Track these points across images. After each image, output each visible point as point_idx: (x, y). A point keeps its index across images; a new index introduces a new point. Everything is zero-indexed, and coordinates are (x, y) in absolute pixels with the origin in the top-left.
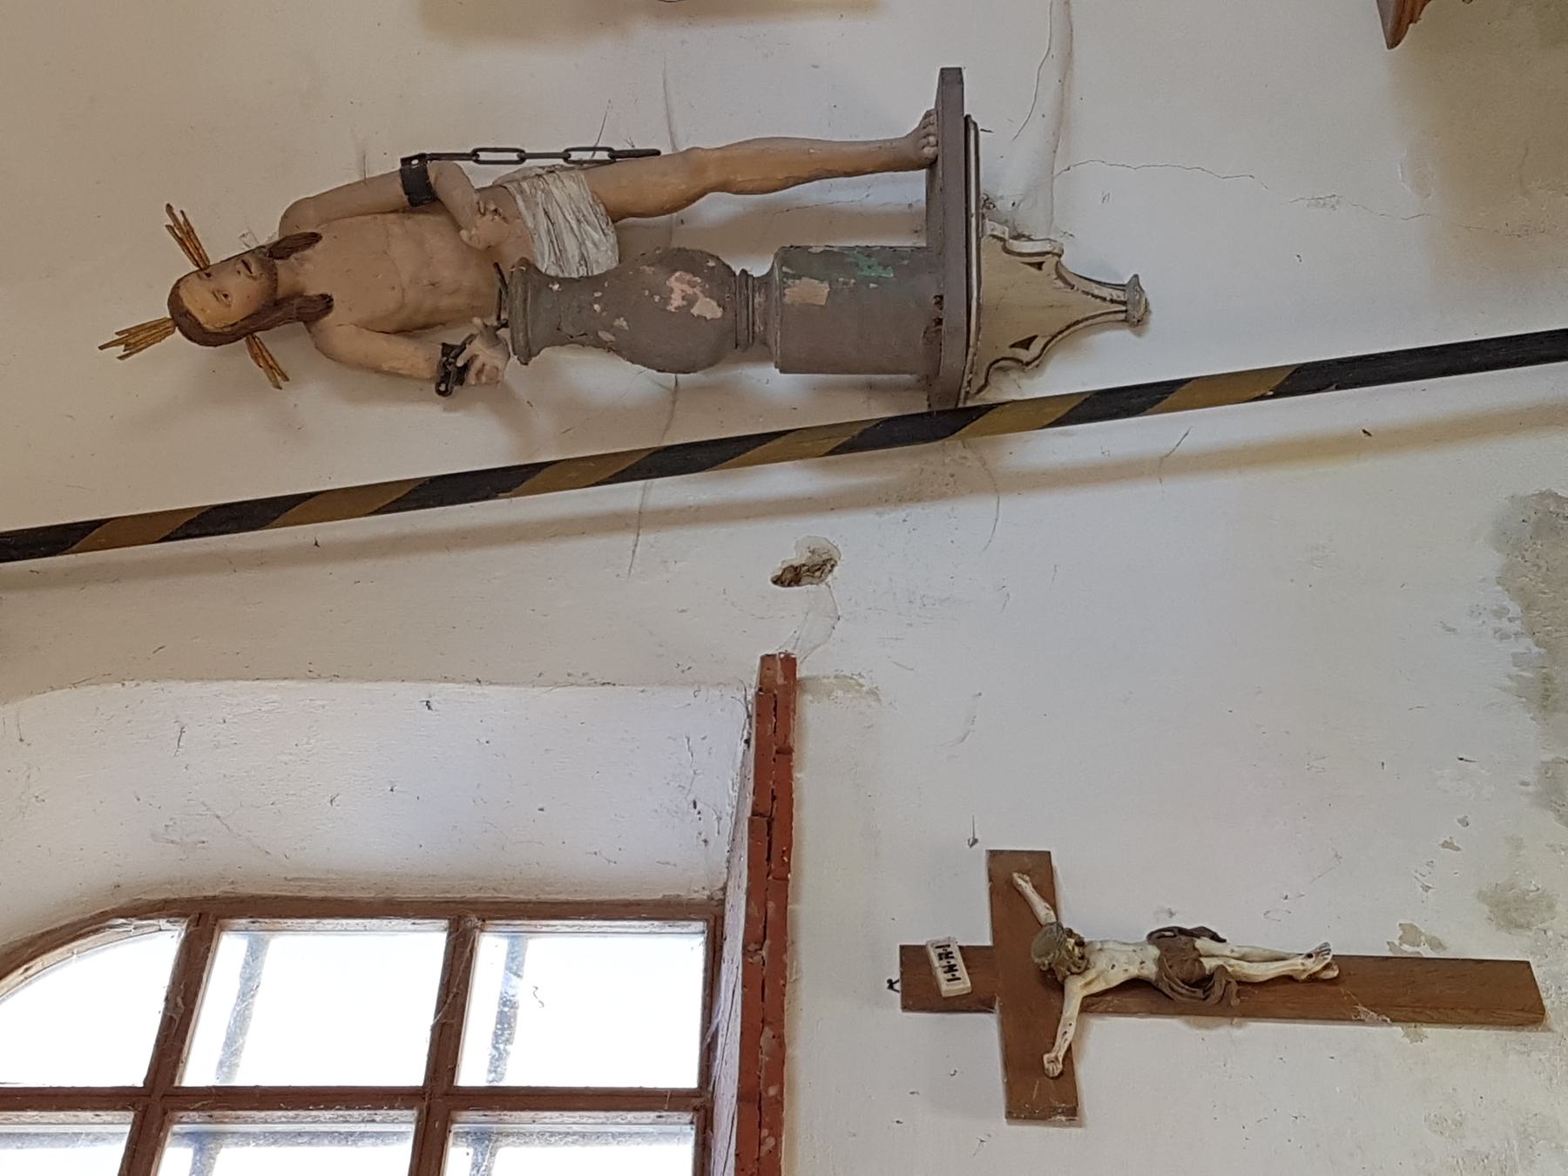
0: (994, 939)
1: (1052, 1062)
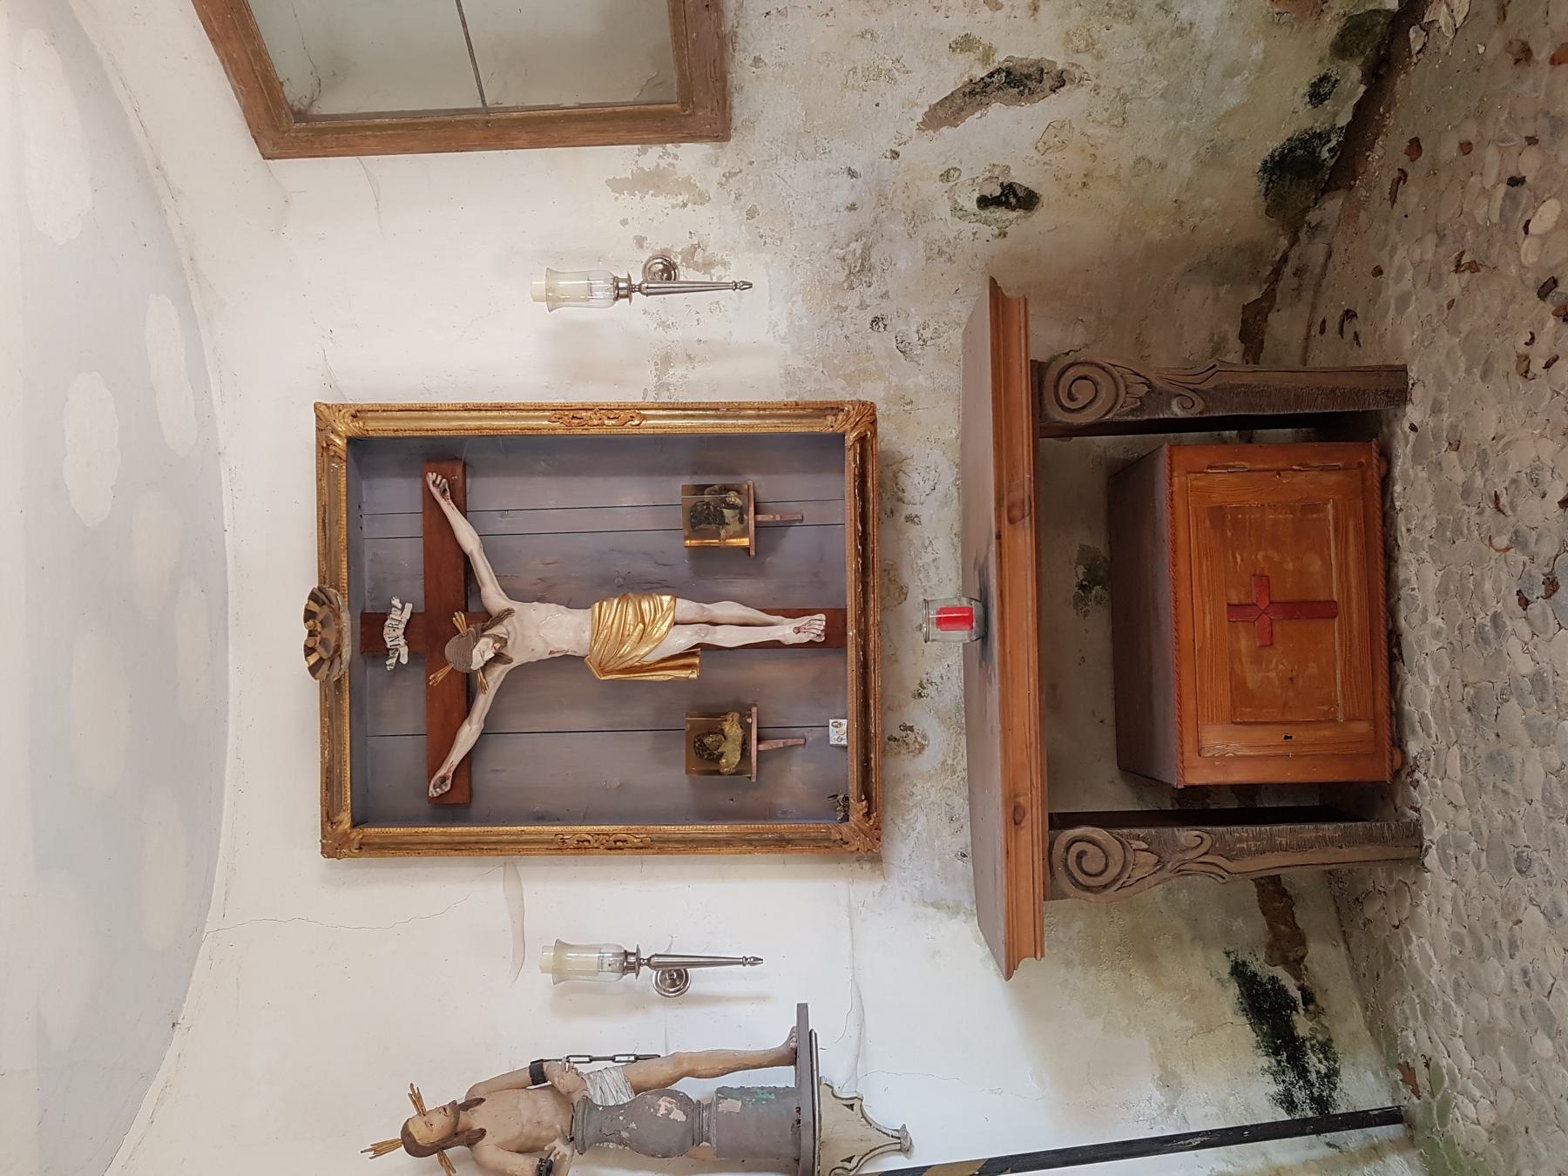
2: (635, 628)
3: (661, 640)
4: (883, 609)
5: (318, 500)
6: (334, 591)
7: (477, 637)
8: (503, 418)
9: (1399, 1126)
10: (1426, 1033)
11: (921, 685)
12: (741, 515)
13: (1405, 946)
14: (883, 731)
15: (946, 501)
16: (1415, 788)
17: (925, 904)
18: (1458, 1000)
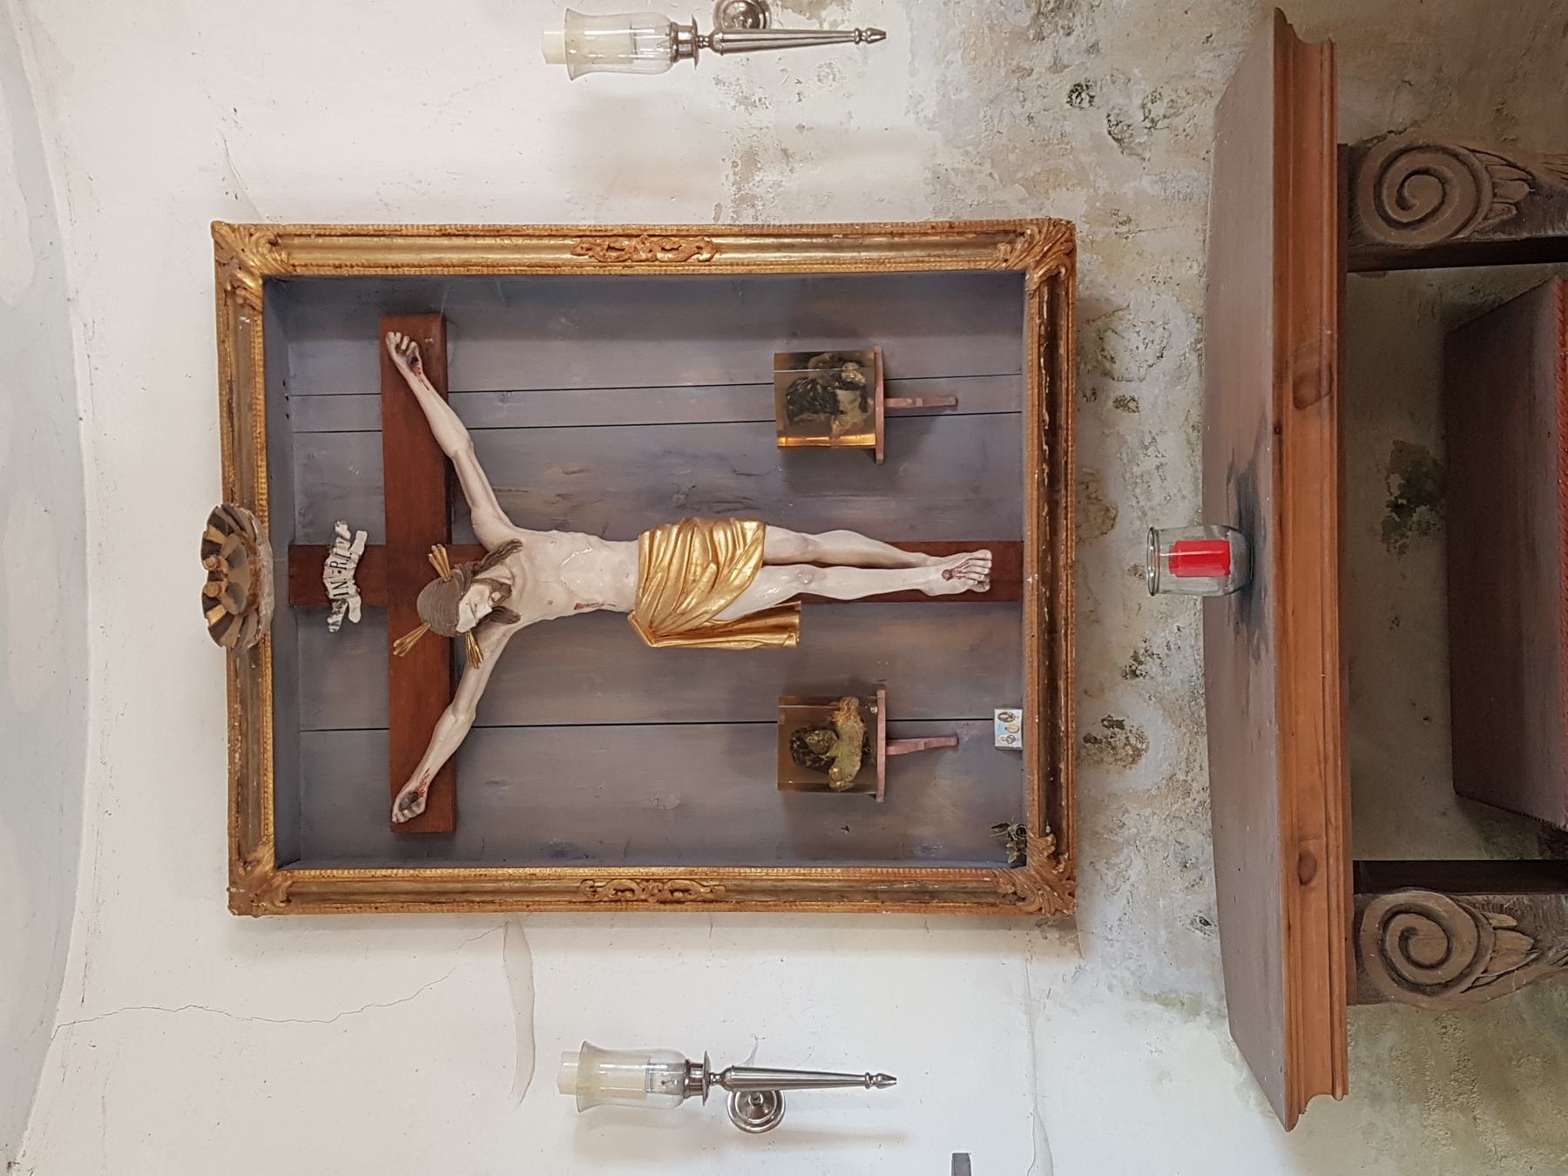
2: (704, 570)
3: (742, 588)
4: (1080, 540)
5: (220, 373)
6: (248, 512)
8: (503, 248)
11: (1135, 658)
12: (864, 398)
14: (1076, 732)
15: (1179, 375)
17: (1145, 997)
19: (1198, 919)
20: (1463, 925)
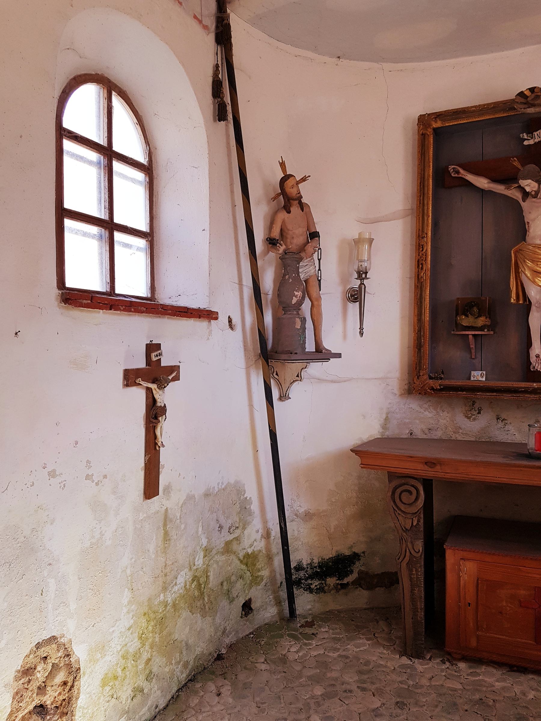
0: (163, 367)
1: (139, 380)
3: (534, 282)
7: (538, 181)
9: (288, 615)
10: (326, 637)
13: (365, 637)
16: (441, 661)
17: (387, 414)
18: (340, 656)
19: (412, 432)
20: (413, 509)
